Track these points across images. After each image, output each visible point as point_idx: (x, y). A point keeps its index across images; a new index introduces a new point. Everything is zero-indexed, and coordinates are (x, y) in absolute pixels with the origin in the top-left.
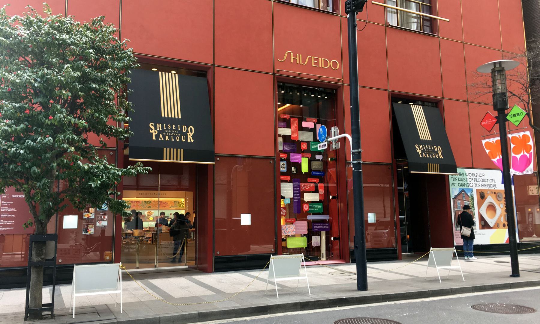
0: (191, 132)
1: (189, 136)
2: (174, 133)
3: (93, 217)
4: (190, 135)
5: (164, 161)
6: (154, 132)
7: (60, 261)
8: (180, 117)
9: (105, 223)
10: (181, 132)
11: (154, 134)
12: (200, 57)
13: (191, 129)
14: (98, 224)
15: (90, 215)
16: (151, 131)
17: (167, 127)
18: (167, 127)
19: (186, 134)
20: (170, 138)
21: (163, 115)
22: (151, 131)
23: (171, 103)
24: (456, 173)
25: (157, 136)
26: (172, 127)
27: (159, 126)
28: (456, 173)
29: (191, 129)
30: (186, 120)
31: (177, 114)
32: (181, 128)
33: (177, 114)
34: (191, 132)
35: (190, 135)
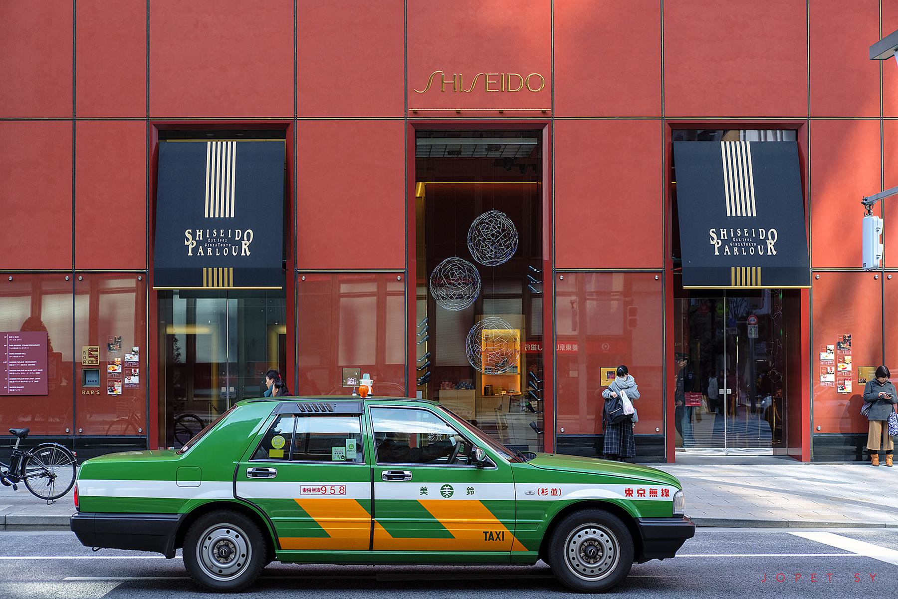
0: (773, 239)
1: (769, 246)
2: (748, 242)
3: (120, 371)
4: (770, 244)
5: (205, 287)
6: (716, 243)
7: (658, 430)
8: (755, 215)
9: (135, 380)
10: (757, 240)
11: (717, 246)
12: (794, 111)
13: (772, 233)
14: (126, 381)
15: (116, 367)
16: (712, 242)
17: (735, 233)
18: (735, 233)
19: (764, 243)
20: (740, 250)
21: (729, 215)
22: (712, 242)
23: (220, 195)
24: (329, 459)
25: (195, 250)
26: (743, 232)
27: (723, 232)
28: (329, 459)
29: (772, 233)
30: (763, 219)
31: (750, 210)
32: (757, 233)
33: (750, 210)
34: (773, 239)
35: (770, 244)
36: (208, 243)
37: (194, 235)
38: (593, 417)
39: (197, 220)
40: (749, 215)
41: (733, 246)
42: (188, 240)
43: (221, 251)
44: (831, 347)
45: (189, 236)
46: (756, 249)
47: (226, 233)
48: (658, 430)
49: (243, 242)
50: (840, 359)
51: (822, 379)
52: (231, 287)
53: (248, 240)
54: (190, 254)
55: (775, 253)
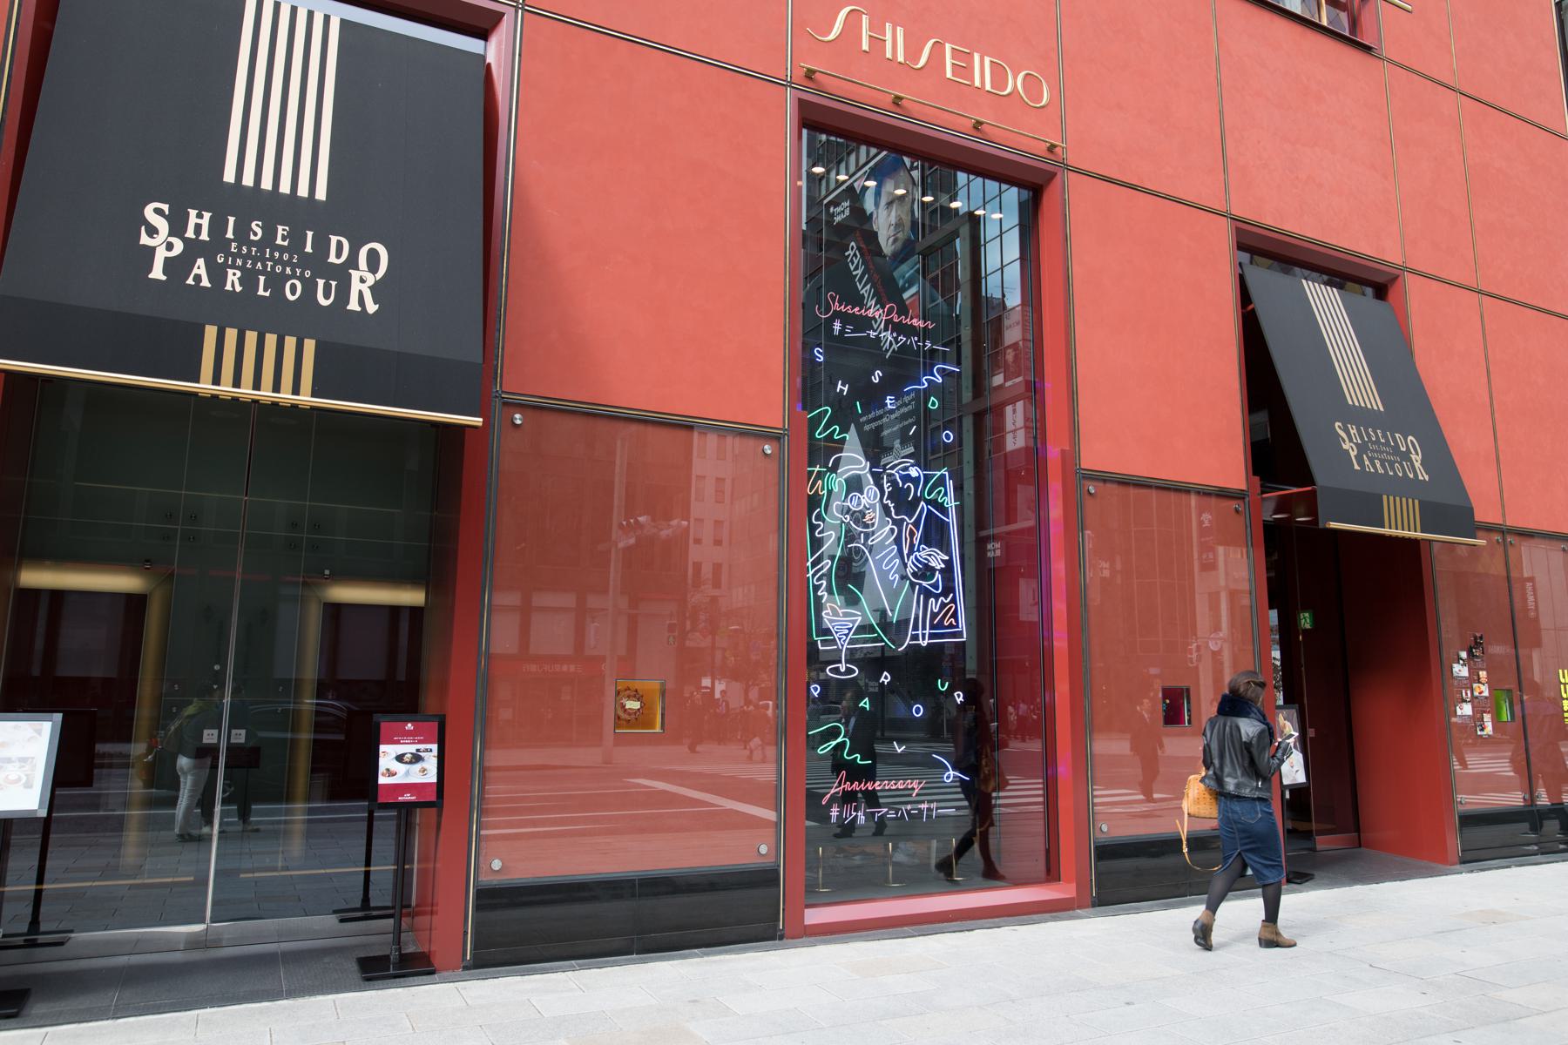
1: (356, 286)
4: (362, 283)
5: (205, 386)
7: (764, 849)
8: (321, 195)
10: (318, 264)
16: (145, 240)
18: (242, 232)
21: (229, 176)
31: (313, 180)
32: (322, 245)
33: (313, 180)
35: (362, 283)
36: (228, 254)
37: (177, 228)
38: (996, 811)
39: (194, 178)
40: (285, 188)
41: (225, 266)
42: (153, 231)
43: (276, 282)
44: (1464, 655)
45: (162, 225)
46: (309, 288)
47: (296, 239)
48: (764, 849)
49: (355, 275)
50: (1474, 678)
51: (1459, 712)
52: (306, 399)
53: (373, 267)
54: (157, 273)
55: (372, 308)
